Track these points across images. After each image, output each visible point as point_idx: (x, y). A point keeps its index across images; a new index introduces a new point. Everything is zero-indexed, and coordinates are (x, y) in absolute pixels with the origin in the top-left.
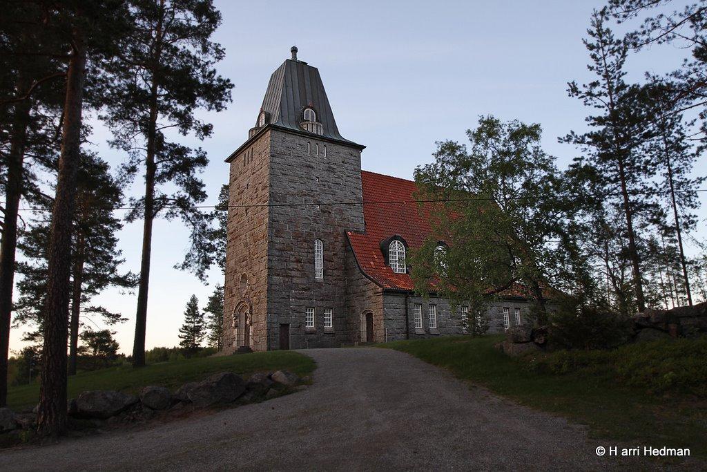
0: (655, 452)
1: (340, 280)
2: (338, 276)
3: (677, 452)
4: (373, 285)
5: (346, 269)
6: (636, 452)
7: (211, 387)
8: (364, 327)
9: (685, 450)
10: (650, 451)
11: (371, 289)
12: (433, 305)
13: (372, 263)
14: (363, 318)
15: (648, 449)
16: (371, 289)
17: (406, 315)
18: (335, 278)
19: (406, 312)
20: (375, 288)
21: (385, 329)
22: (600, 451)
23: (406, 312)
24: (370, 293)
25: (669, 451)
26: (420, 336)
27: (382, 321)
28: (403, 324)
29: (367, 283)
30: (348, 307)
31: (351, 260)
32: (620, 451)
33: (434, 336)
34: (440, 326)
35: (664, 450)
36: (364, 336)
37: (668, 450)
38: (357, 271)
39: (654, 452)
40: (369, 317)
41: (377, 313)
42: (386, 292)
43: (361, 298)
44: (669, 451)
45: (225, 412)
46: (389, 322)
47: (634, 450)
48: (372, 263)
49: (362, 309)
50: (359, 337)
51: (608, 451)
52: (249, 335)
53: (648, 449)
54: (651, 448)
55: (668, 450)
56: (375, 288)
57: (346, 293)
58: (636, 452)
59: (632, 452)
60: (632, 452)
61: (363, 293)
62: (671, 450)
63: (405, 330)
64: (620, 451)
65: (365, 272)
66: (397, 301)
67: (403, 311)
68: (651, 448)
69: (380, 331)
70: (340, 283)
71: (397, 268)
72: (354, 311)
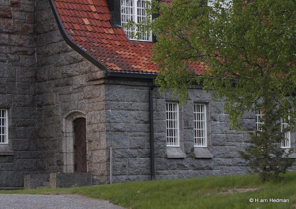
0: (274, 201)
1: (25, 53)
2: (21, 46)
3: (283, 201)
4: (87, 65)
5: (36, 33)
6: (266, 201)
7: (279, 139)
8: (68, 145)
9: (287, 200)
10: (272, 200)
11: (81, 72)
12: (200, 104)
13: (86, 21)
14: (68, 127)
15: (271, 199)
16: (81, 72)
17: (150, 122)
18: (14, 50)
19: (150, 116)
20: (91, 71)
21: (108, 149)
22: (251, 200)
23: (150, 116)
24: (80, 80)
25: (280, 200)
26: (175, 162)
27: (104, 135)
28: (142, 140)
29: (76, 61)
30: (39, 106)
31: (46, 15)
32: (259, 200)
33: (202, 162)
34: (213, 144)
35: (278, 200)
36: (69, 161)
37: (280, 200)
38: (57, 36)
39: (274, 201)
40: (79, 124)
41: (95, 118)
42: (112, 79)
43: (65, 90)
44: (280, 200)
45: (87, 199)
46: (117, 136)
47: (266, 200)
48: (86, 21)
49: (65, 110)
50: (60, 163)
51: (254, 200)
52: (76, 158)
53: (271, 199)
54: (272, 199)
55: (280, 200)
56: (91, 71)
57: (36, 79)
58: (266, 201)
59: (265, 200)
60: (265, 200)
61: (67, 80)
62: (281, 200)
63: (146, 150)
64: (259, 200)
65: (72, 39)
66: (133, 96)
67: (145, 116)
68: (272, 199)
69: (98, 155)
70: (26, 61)
71: (133, 33)
72: (50, 114)
